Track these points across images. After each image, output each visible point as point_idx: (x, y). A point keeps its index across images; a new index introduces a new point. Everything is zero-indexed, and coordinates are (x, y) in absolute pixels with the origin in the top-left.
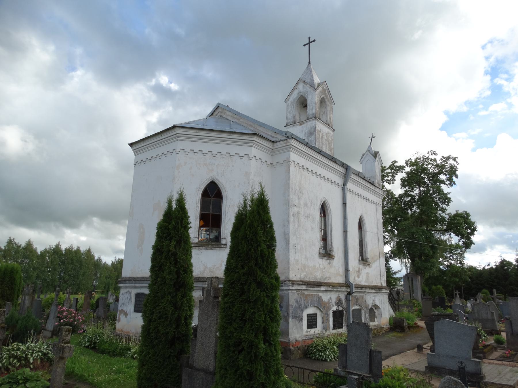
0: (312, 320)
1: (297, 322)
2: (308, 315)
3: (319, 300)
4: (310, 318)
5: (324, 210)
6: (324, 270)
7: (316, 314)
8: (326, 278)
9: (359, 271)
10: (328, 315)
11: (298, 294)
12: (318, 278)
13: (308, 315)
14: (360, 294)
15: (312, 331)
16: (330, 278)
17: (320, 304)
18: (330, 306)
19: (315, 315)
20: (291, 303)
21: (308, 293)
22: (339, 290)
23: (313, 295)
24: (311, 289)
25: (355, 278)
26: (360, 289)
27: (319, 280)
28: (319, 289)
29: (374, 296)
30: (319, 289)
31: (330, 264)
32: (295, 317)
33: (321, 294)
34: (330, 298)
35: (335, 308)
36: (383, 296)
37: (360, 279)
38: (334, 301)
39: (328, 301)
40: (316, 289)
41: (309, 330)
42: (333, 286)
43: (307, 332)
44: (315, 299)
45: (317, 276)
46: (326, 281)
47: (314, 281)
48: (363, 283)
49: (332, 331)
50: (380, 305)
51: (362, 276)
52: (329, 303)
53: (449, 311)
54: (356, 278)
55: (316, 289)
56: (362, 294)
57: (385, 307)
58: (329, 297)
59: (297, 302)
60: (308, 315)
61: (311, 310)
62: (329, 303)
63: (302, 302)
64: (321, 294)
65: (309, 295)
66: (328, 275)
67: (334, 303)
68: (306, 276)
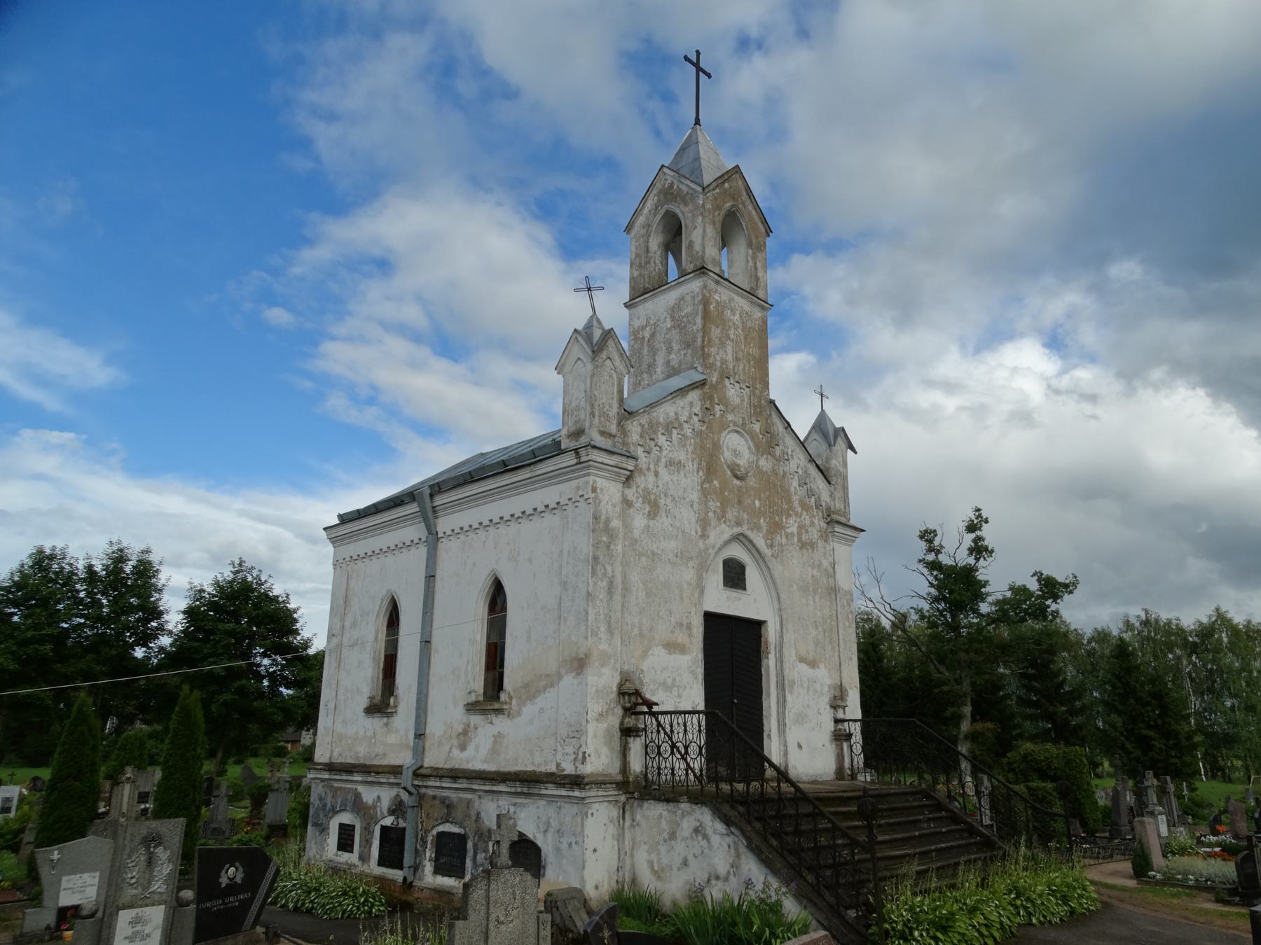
0: (345, 836)
1: (317, 834)
2: (342, 826)
3: (355, 799)
4: (343, 831)
5: (393, 621)
6: (373, 740)
7: (354, 826)
8: (377, 755)
9: (465, 733)
10: (371, 833)
11: (323, 787)
12: (360, 755)
13: (340, 824)
14: (461, 795)
15: (345, 857)
16: (385, 755)
17: (357, 805)
18: (376, 814)
19: (352, 827)
20: (312, 800)
21: (339, 785)
22: (392, 780)
23: (346, 788)
24: (338, 777)
25: (450, 752)
26: (449, 780)
27: (362, 761)
28: (351, 778)
29: (515, 804)
30: (351, 778)
31: (387, 725)
32: (315, 825)
33: (361, 788)
34: (379, 797)
35: (388, 821)
36: (560, 808)
37: (470, 750)
38: (385, 803)
39: (373, 804)
40: (345, 777)
41: (340, 853)
42: (377, 773)
43: (336, 855)
44: (349, 797)
45: (361, 753)
46: (376, 762)
47: (353, 762)
48: (477, 765)
49: (374, 868)
50: (538, 836)
51: (477, 748)
52: (374, 807)
53: (496, 706)
54: (456, 752)
55: (345, 777)
56: (468, 796)
57: (564, 846)
58: (375, 795)
59: (321, 799)
60: (342, 826)
61: (346, 818)
62: (374, 807)
63: (329, 801)
64: (361, 788)
65: (341, 789)
66: (379, 749)
67: (385, 810)
68: (340, 755)
